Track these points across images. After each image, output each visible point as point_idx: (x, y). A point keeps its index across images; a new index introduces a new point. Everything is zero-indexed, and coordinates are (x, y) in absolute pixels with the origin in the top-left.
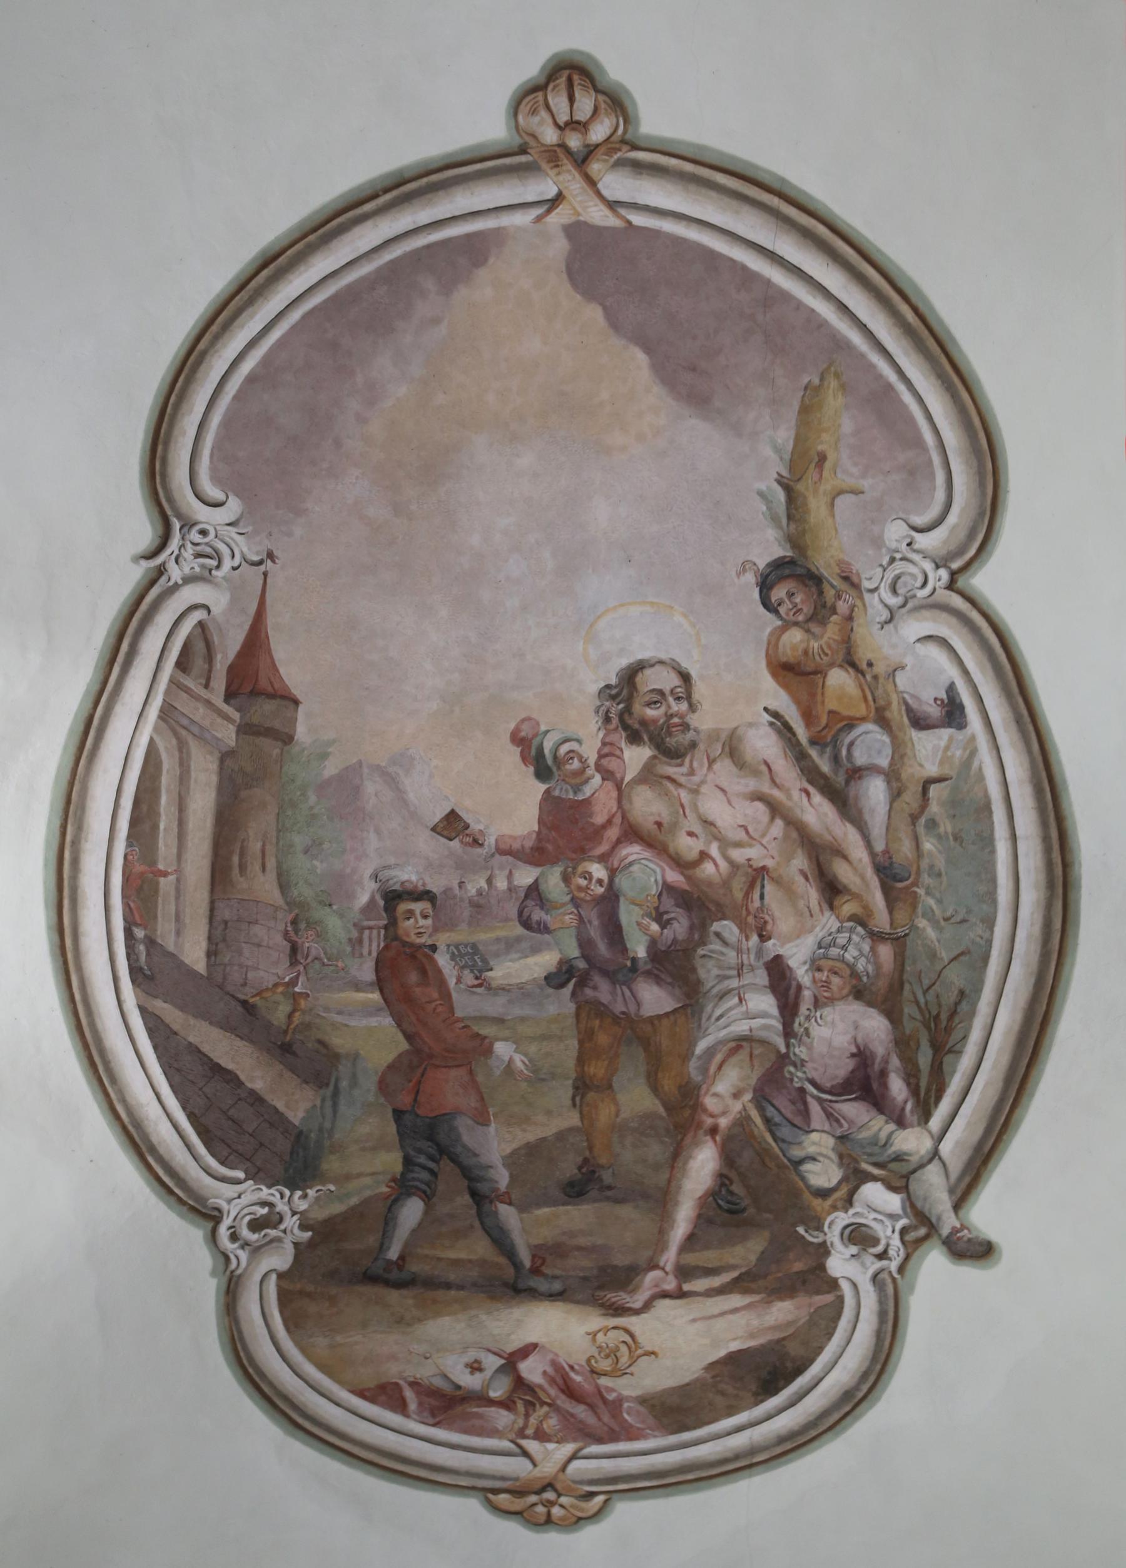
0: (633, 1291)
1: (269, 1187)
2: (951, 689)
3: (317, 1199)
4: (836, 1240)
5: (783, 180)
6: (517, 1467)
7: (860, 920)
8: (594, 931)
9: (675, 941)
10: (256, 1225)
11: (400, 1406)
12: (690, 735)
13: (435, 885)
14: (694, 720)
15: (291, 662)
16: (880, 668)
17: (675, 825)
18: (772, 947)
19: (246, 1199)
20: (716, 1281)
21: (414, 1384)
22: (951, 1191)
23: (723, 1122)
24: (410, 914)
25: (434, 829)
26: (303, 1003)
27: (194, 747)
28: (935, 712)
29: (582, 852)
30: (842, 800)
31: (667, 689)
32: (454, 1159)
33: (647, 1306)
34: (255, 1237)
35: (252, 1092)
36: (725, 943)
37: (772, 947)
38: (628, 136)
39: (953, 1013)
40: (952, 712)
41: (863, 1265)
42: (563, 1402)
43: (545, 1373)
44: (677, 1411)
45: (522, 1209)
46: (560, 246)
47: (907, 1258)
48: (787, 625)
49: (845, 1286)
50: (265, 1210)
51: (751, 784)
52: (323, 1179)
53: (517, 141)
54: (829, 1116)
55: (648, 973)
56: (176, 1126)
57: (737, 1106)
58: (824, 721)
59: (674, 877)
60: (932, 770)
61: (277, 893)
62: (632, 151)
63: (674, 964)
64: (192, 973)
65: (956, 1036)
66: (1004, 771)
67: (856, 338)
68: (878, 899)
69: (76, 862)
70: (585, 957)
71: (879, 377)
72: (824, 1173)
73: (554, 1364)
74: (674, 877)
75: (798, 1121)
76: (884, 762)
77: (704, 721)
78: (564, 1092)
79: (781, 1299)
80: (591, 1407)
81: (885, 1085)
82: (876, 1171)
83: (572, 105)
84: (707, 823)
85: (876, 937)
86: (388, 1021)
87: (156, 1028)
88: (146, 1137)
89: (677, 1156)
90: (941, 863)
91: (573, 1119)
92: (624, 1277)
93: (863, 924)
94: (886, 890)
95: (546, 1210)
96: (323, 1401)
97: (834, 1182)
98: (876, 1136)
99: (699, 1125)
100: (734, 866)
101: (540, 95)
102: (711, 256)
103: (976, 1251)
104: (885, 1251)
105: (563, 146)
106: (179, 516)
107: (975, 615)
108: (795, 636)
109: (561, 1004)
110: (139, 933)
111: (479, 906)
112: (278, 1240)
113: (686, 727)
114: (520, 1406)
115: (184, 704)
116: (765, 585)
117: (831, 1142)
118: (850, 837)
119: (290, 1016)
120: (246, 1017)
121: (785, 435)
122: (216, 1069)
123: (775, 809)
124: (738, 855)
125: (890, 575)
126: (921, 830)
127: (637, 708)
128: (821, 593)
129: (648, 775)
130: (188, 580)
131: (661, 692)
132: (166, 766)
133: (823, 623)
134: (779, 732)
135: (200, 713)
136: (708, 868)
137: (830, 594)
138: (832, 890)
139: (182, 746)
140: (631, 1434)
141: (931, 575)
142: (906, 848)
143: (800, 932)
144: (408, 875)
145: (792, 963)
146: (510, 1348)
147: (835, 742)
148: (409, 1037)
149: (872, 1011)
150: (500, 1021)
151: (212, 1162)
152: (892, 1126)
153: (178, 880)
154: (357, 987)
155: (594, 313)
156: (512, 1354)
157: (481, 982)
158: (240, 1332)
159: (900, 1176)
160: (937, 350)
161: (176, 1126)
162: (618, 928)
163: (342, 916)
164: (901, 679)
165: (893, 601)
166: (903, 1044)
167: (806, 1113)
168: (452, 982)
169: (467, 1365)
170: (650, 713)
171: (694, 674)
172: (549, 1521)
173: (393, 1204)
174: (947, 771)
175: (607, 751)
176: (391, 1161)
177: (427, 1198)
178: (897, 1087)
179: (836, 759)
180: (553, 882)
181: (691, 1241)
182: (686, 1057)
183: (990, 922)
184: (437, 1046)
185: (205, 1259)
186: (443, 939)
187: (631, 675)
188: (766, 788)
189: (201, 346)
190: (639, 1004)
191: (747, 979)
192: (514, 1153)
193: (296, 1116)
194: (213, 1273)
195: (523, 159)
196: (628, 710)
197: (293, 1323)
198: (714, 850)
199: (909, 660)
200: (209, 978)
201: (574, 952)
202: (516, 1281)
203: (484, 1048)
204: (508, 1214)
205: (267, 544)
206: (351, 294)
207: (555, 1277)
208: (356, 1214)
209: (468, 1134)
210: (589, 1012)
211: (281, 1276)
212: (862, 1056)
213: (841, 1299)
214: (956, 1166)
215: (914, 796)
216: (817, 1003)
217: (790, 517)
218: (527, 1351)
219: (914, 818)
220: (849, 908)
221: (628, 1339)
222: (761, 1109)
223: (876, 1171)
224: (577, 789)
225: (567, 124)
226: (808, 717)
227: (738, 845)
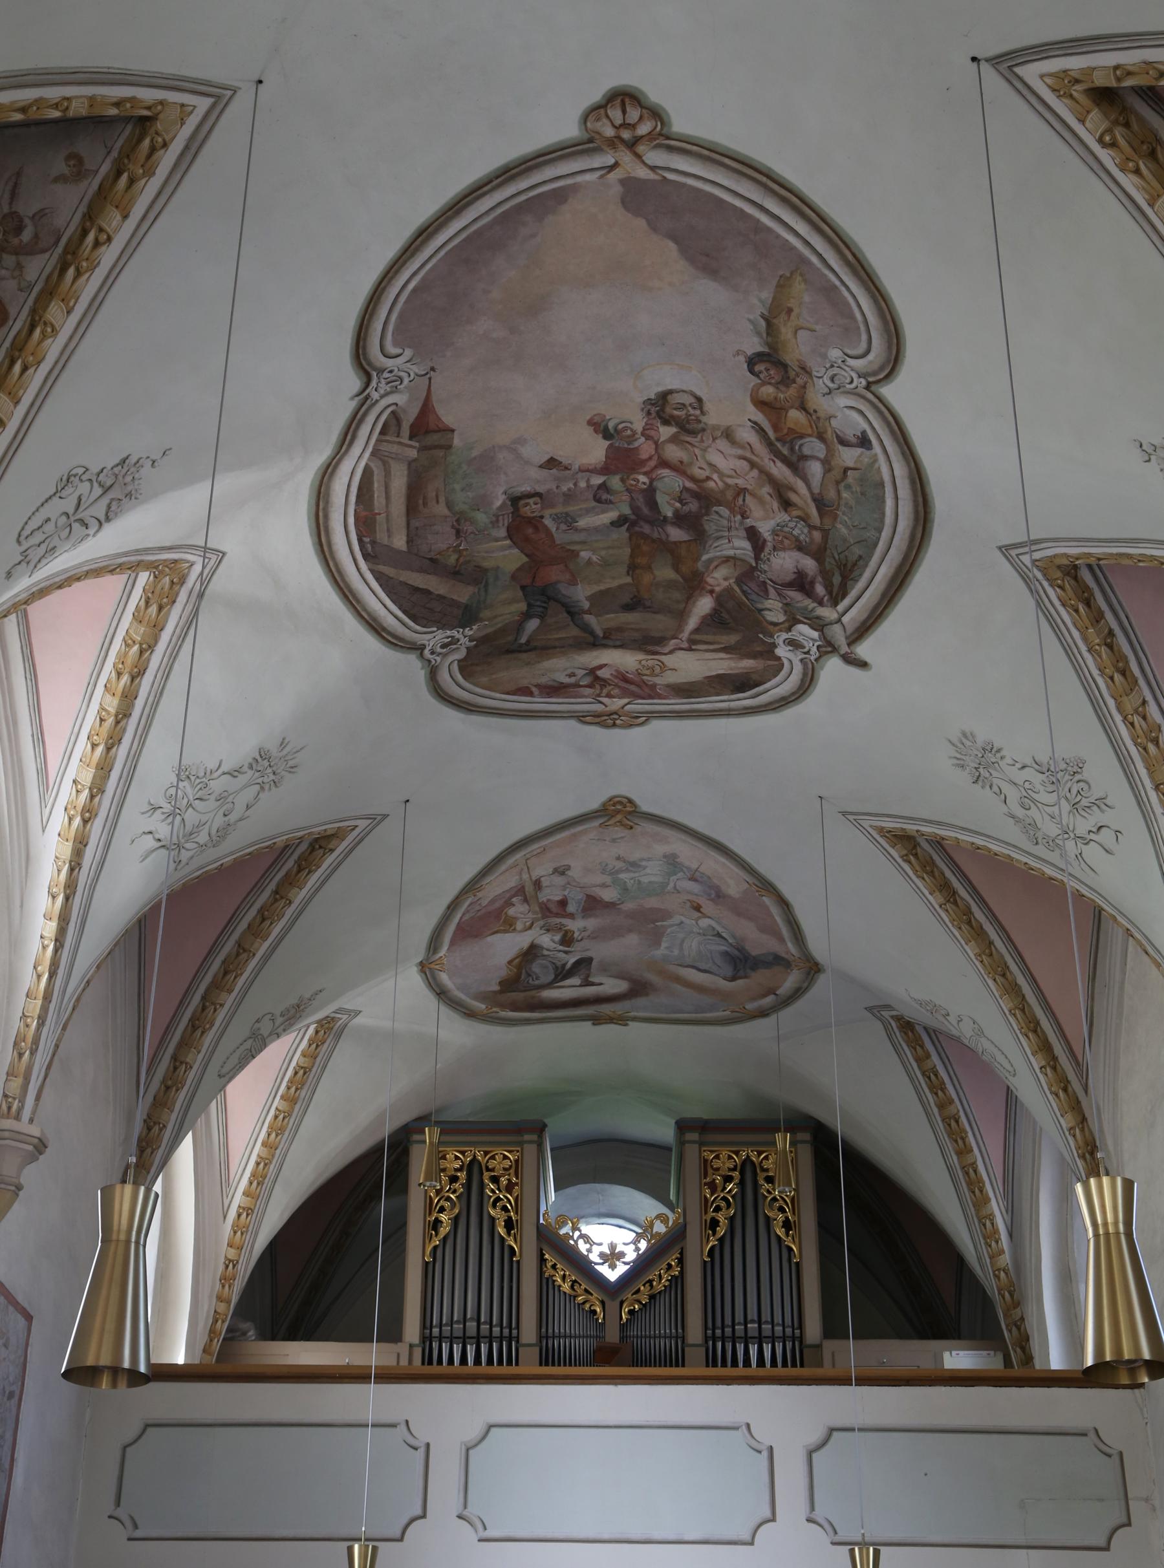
2: (864, 433)
4: (781, 643)
5: (770, 169)
6: (598, 708)
11: (531, 694)
13: (540, 489)
14: (704, 419)
15: (447, 415)
16: (821, 414)
17: (691, 464)
20: (712, 647)
22: (847, 638)
23: (717, 589)
24: (527, 504)
25: (540, 467)
28: (854, 440)
30: (796, 463)
31: (687, 403)
32: (556, 600)
33: (671, 652)
35: (438, 595)
36: (721, 516)
37: (749, 522)
38: (664, 132)
39: (855, 564)
40: (864, 442)
42: (622, 684)
44: (686, 690)
45: (596, 616)
46: (617, 189)
47: (820, 657)
48: (764, 383)
51: (740, 452)
52: (482, 620)
53: (586, 136)
54: (779, 594)
55: (673, 524)
56: (396, 617)
57: (726, 584)
58: (785, 431)
62: (664, 138)
63: (690, 521)
64: (399, 552)
65: (856, 573)
67: (814, 259)
68: (814, 512)
69: (326, 517)
71: (829, 281)
78: (623, 569)
80: (638, 686)
83: (625, 119)
84: (710, 464)
85: (812, 528)
86: (516, 551)
87: (378, 576)
90: (852, 503)
92: (661, 641)
94: (819, 509)
99: (703, 588)
100: (727, 486)
101: (602, 111)
105: (619, 137)
106: (375, 369)
109: (622, 533)
110: (367, 540)
111: (569, 497)
114: (598, 686)
116: (752, 362)
118: (800, 485)
119: (457, 560)
120: (433, 565)
121: (767, 295)
122: (417, 589)
123: (753, 465)
125: (831, 372)
127: (668, 410)
128: (787, 372)
129: (674, 439)
130: (382, 397)
131: (684, 405)
133: (788, 386)
134: (757, 431)
136: (711, 484)
137: (792, 374)
138: (786, 504)
139: (385, 463)
140: (660, 697)
141: (855, 380)
143: (766, 518)
147: (792, 442)
150: (584, 543)
151: (418, 628)
152: (815, 605)
154: (497, 540)
155: (641, 223)
159: (819, 625)
160: (865, 277)
161: (396, 617)
162: (656, 503)
163: (485, 513)
164: (834, 422)
165: (831, 385)
167: (766, 592)
168: (554, 530)
170: (676, 413)
171: (704, 398)
172: (614, 725)
174: (858, 466)
177: (542, 617)
178: (820, 589)
179: (792, 449)
180: (615, 482)
181: (697, 631)
182: (698, 559)
183: (880, 530)
186: (547, 513)
187: (664, 396)
188: (748, 455)
189: (383, 285)
190: (668, 536)
191: (734, 533)
195: (591, 145)
196: (663, 410)
198: (715, 477)
200: (409, 551)
201: (627, 511)
203: (575, 554)
204: (591, 620)
205: (430, 364)
206: (479, 233)
208: (503, 631)
209: (564, 590)
210: (636, 538)
214: (850, 630)
216: (775, 548)
217: (768, 334)
218: (601, 667)
219: (838, 483)
220: (795, 513)
222: (739, 586)
225: (621, 125)
226: (776, 428)
227: (729, 476)
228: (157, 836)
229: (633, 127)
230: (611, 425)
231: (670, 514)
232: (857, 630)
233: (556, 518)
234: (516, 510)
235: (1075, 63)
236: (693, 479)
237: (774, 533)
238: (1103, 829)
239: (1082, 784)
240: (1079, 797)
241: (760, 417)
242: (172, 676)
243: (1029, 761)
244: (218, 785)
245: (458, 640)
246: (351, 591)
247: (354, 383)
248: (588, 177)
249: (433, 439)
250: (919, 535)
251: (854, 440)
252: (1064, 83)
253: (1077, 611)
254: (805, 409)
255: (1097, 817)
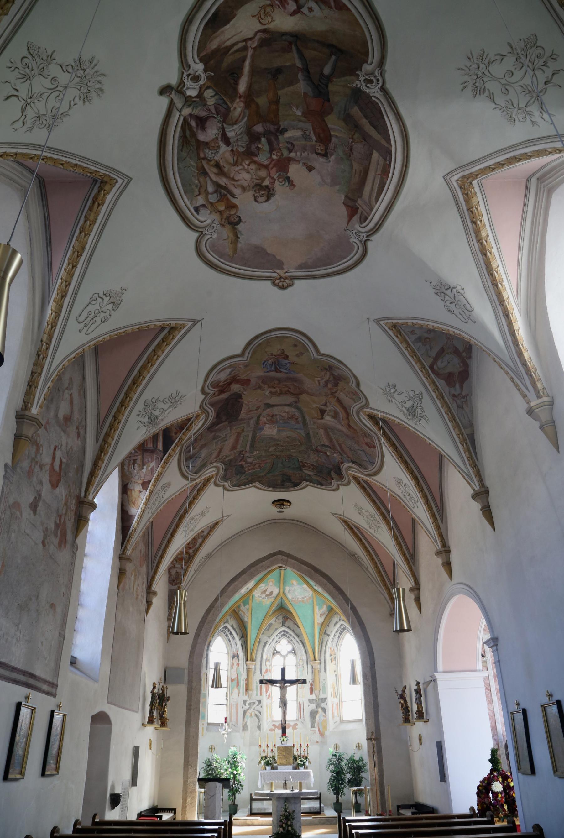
0: (260, 39)
1: (366, 92)
2: (198, 214)
3: (353, 83)
4: (202, 75)
7: (210, 161)
8: (275, 143)
9: (254, 144)
10: (371, 82)
12: (254, 189)
13: (315, 156)
14: (253, 193)
15: (343, 211)
16: (214, 213)
18: (230, 148)
19: (373, 91)
20: (236, 48)
21: (331, 7)
22: (174, 104)
23: (238, 100)
24: (322, 150)
26: (351, 136)
27: (367, 201)
28: (201, 209)
29: (278, 161)
30: (218, 186)
32: (313, 83)
33: (256, 34)
34: (372, 78)
35: (367, 119)
36: (242, 146)
37: (230, 148)
39: (183, 146)
40: (197, 210)
41: (193, 70)
43: (288, 4)
45: (295, 65)
46: (284, 267)
47: (182, 78)
48: (235, 214)
49: (197, 61)
50: (368, 85)
51: (239, 183)
54: (210, 110)
56: (388, 117)
57: (235, 105)
59: (256, 159)
60: (199, 197)
61: (354, 164)
62: (273, 280)
63: (254, 138)
64: (377, 150)
65: (181, 141)
66: (184, 202)
70: (277, 136)
72: (209, 93)
73: (285, 8)
74: (256, 159)
75: (218, 106)
76: (210, 196)
77: (251, 193)
79: (215, 49)
81: (196, 123)
82: (195, 99)
84: (248, 172)
85: (205, 158)
86: (329, 126)
87: (389, 141)
88: (396, 117)
89: (250, 87)
90: (193, 179)
91: (280, 92)
92: (263, 43)
93: (209, 160)
94: (204, 169)
95: (287, 64)
96: (360, 11)
97: (205, 92)
98: (196, 109)
102: (256, 268)
103: (165, 90)
104: (188, 77)
107: (196, 229)
108: (232, 213)
110: (388, 162)
111: (304, 149)
112: (367, 75)
113: (255, 191)
115: (368, 210)
116: (240, 220)
117: (208, 103)
120: (365, 137)
121: (239, 245)
122: (375, 127)
123: (233, 179)
124: (240, 167)
126: (199, 185)
127: (266, 193)
129: (263, 179)
130: (362, 233)
131: (261, 197)
132: (374, 198)
135: (365, 207)
136: (247, 162)
137: (227, 222)
142: (202, 180)
143: (224, 153)
144: (321, 159)
145: (225, 146)
146: (299, 15)
147: (221, 196)
148: (324, 121)
149: (203, 140)
150: (300, 121)
152: (193, 113)
153: (376, 172)
154: (336, 136)
155: (278, 257)
156: (298, 12)
157: (304, 131)
158: (381, 48)
159: (189, 101)
161: (388, 117)
164: (209, 212)
166: (194, 135)
167: (216, 109)
168: (312, 132)
169: (313, 11)
170: (263, 192)
173: (332, 74)
175: (273, 183)
176: (331, 88)
177: (322, 74)
178: (193, 123)
179: (220, 193)
180: (285, 153)
181: (244, 60)
182: (249, 115)
183: (179, 168)
184: (317, 115)
185: (387, 76)
186: (314, 143)
187: (268, 199)
188: (235, 183)
190: (263, 126)
191: (235, 139)
192: (297, 83)
193: (356, 109)
194: (386, 71)
196: (268, 192)
197: (365, 44)
198: (246, 167)
199: (208, 216)
201: (280, 137)
202: (296, 39)
203: (304, 114)
204: (299, 64)
207: (285, 41)
210: (276, 123)
211: (367, 62)
212: (204, 128)
213: (198, 56)
214: (175, 110)
215: (203, 190)
216: (217, 138)
218: (294, 13)
219: (201, 186)
220: (212, 163)
221: (261, 21)
223: (195, 99)
224: (280, 175)
226: (228, 199)
227: (241, 170)
228: (541, 114)
229: (281, 282)
230: (287, 184)
231: (263, 139)
232: (171, 113)
233: (310, 139)
234: (326, 149)
235: (183, 331)
236: (255, 162)
237: (219, 147)
238: (22, 125)
239: (43, 125)
240: (41, 122)
241: (234, 201)
242: (490, 153)
243: (70, 112)
244: (501, 100)
245: (364, 80)
246: (403, 137)
247: (369, 244)
248: (293, 271)
249: (351, 204)
250: (163, 172)
251: (201, 209)
252: (183, 326)
253: (91, 173)
254: (219, 211)
255: (29, 123)
